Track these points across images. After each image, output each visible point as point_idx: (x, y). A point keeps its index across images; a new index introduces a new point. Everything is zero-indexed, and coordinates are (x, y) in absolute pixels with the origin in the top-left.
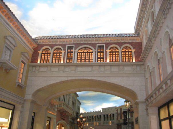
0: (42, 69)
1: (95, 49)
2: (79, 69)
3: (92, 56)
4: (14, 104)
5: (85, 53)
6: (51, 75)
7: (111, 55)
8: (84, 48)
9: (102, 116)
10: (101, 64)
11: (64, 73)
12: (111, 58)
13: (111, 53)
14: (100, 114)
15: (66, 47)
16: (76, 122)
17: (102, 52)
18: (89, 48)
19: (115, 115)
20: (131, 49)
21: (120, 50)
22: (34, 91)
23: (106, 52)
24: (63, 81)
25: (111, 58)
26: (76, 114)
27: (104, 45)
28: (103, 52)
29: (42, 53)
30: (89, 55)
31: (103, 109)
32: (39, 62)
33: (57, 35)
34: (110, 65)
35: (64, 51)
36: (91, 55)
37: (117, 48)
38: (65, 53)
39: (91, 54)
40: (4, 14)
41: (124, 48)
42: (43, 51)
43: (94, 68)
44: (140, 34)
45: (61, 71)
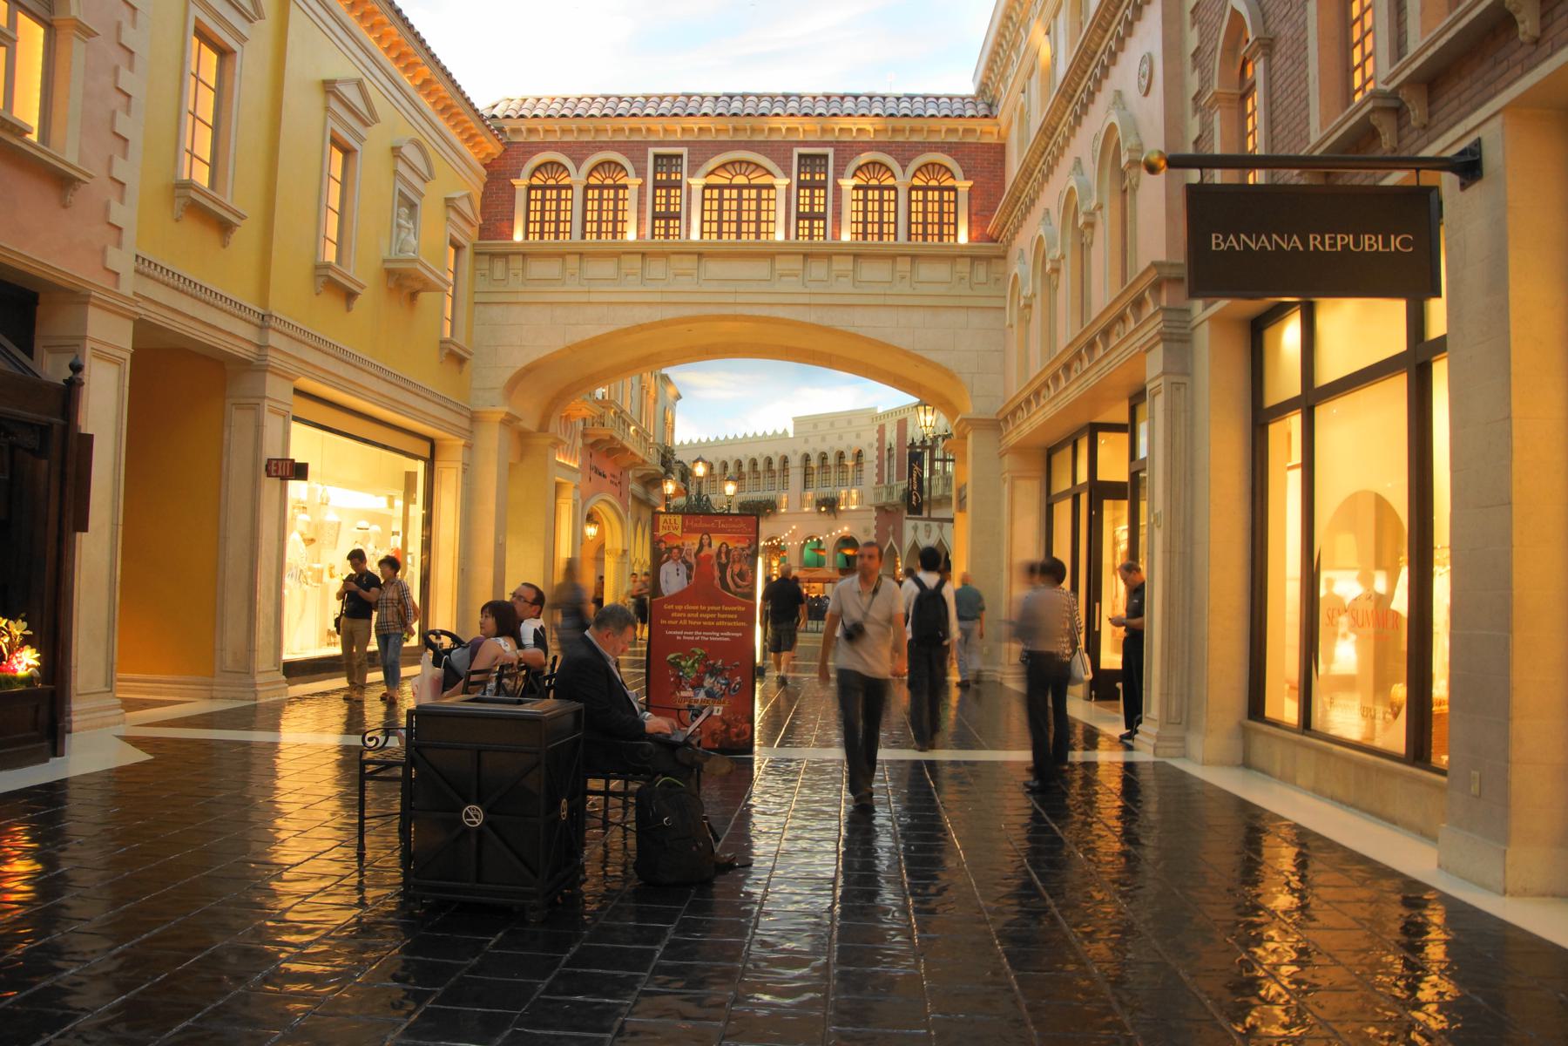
0: (538, 269)
2: (714, 268)
3: (772, 194)
5: (740, 187)
6: (584, 298)
7: (861, 204)
8: (733, 163)
10: (815, 249)
11: (641, 288)
12: (860, 219)
13: (861, 192)
14: (784, 450)
16: (655, 498)
17: (820, 188)
18: (758, 166)
20: (953, 176)
21: (902, 180)
22: (514, 371)
23: (837, 188)
24: (641, 323)
25: (861, 215)
26: (664, 456)
27: (830, 151)
28: (823, 186)
29: (530, 188)
30: (759, 199)
31: (798, 422)
32: (518, 236)
34: (857, 255)
35: (640, 181)
36: (769, 199)
37: (888, 169)
38: (642, 187)
39: (764, 194)
40: (439, 108)
41: (919, 169)
43: (782, 264)
44: (1000, 107)
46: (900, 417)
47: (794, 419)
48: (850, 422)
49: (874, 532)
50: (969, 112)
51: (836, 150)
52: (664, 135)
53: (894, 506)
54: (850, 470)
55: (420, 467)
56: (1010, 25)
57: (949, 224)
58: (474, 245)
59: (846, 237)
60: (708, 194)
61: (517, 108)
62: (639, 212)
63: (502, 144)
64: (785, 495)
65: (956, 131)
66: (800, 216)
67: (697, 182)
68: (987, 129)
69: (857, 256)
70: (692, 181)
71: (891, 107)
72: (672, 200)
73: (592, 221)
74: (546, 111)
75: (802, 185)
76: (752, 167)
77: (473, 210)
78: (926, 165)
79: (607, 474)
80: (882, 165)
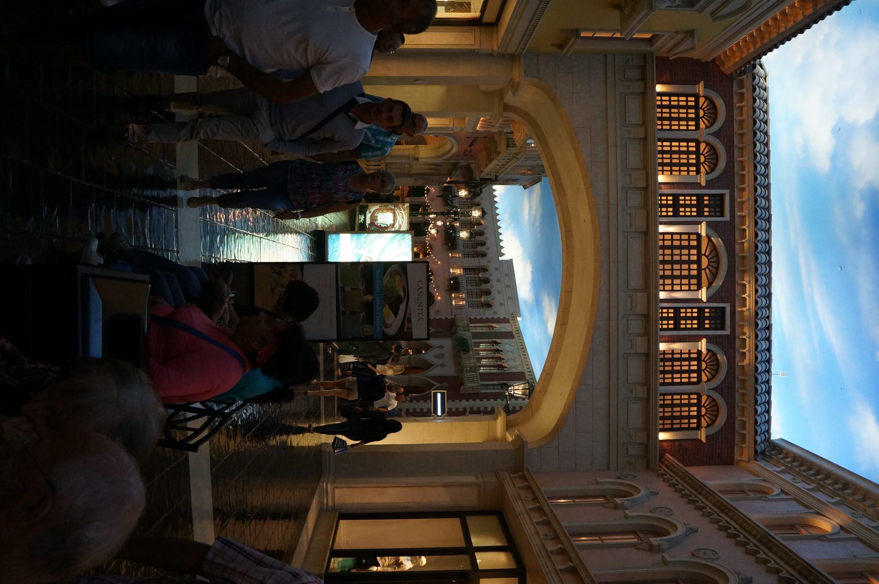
0: (634, 104)
1: (710, 184)
2: (636, 244)
4: (501, 21)
5: (698, 262)
9: (483, 262)
12: (686, 168)
14: (491, 254)
15: (718, 188)
17: (697, 212)
19: (488, 314)
23: (698, 339)
27: (727, 332)
28: (701, 326)
31: (510, 263)
32: (659, 88)
33: (771, 149)
34: (650, 355)
35: (703, 184)
37: (714, 376)
38: (698, 185)
39: (694, 281)
41: (714, 400)
42: (706, 98)
43: (640, 297)
45: (628, 178)
46: (514, 333)
47: (511, 260)
48: (510, 298)
49: (438, 318)
50: (758, 439)
51: (728, 336)
52: (739, 202)
53: (455, 332)
54: (479, 300)
55: (474, 14)
56: (837, 486)
57: (672, 424)
58: (652, 53)
59: (663, 346)
60: (694, 237)
61: (760, 85)
62: (679, 183)
63: (732, 74)
64: (460, 255)
65: (744, 428)
66: (677, 327)
67: (703, 229)
68: (746, 452)
69: (647, 355)
70: (704, 225)
71: (762, 378)
72: (688, 209)
73: (671, 146)
74: (758, 107)
75: (701, 310)
76: (714, 271)
77: (683, 50)
78: (717, 405)
79: (471, 148)
80: (717, 371)
